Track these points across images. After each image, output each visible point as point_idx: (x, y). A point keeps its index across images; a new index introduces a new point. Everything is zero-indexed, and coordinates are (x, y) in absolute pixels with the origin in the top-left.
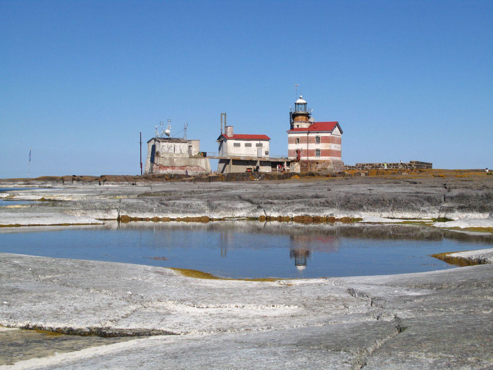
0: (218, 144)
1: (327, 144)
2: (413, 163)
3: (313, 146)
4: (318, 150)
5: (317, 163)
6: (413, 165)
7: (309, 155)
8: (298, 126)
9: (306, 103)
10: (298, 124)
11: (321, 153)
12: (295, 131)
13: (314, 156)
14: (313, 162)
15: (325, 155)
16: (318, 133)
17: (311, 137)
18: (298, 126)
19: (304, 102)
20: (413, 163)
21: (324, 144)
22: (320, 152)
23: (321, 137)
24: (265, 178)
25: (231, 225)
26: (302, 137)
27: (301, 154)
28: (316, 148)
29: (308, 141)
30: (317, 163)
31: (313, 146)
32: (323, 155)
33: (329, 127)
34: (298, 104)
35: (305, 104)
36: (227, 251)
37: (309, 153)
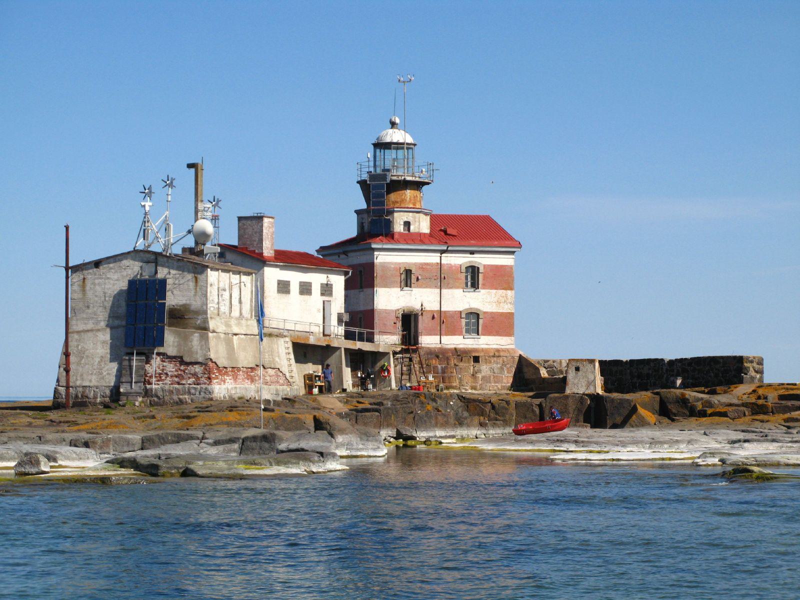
0: (425, 188)
1: (501, 292)
2: (752, 362)
3: (458, 300)
4: (474, 314)
5: (476, 359)
6: (751, 369)
7: (443, 332)
8: (407, 224)
9: (415, 145)
10: (409, 217)
11: (484, 323)
12: (398, 242)
13: (460, 334)
14: (460, 354)
15: (498, 333)
16: (472, 253)
17: (450, 267)
18: (407, 224)
19: (409, 139)
20: (752, 362)
21: (494, 291)
22: (481, 321)
23: (484, 266)
24: (199, 276)
25: (225, 397)
26: (423, 267)
27: (423, 323)
28: (467, 306)
29: (441, 278)
30: (476, 359)
31: (458, 300)
32: (489, 332)
33: (481, 231)
34: (387, 146)
35: (410, 147)
36: (214, 361)
37: (444, 322)
